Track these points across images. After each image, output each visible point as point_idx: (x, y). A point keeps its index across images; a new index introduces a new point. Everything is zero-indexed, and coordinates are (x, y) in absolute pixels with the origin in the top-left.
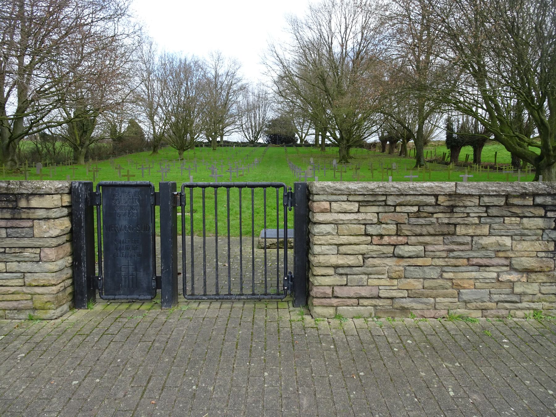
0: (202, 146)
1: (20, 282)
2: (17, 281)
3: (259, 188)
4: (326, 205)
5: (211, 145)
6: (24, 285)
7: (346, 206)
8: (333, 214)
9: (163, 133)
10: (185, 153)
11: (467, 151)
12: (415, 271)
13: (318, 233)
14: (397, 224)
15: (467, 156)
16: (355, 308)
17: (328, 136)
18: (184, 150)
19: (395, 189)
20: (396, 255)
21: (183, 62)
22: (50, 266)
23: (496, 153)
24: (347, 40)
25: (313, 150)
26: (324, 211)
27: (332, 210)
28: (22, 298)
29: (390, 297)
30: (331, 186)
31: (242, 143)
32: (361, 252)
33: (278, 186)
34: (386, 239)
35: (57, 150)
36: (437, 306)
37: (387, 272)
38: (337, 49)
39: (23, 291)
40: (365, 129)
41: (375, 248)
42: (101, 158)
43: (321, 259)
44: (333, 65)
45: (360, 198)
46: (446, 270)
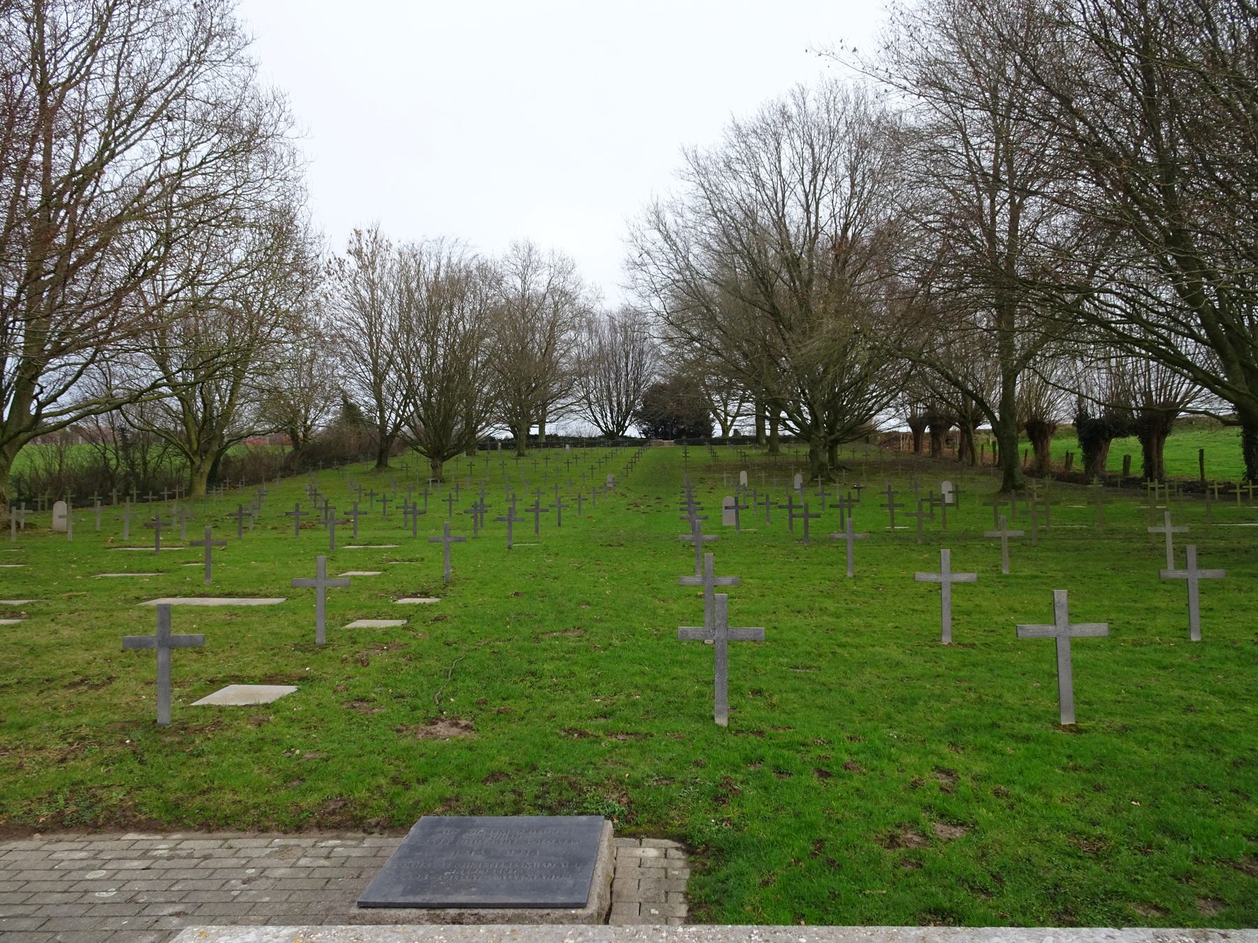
0: (494, 447)
10: (449, 466)
15: (1127, 460)
17: (784, 419)
18: (444, 459)
23: (1202, 452)
24: (819, 199)
25: (748, 452)
31: (590, 438)
35: (152, 465)
38: (794, 213)
40: (870, 400)
44: (793, 263)
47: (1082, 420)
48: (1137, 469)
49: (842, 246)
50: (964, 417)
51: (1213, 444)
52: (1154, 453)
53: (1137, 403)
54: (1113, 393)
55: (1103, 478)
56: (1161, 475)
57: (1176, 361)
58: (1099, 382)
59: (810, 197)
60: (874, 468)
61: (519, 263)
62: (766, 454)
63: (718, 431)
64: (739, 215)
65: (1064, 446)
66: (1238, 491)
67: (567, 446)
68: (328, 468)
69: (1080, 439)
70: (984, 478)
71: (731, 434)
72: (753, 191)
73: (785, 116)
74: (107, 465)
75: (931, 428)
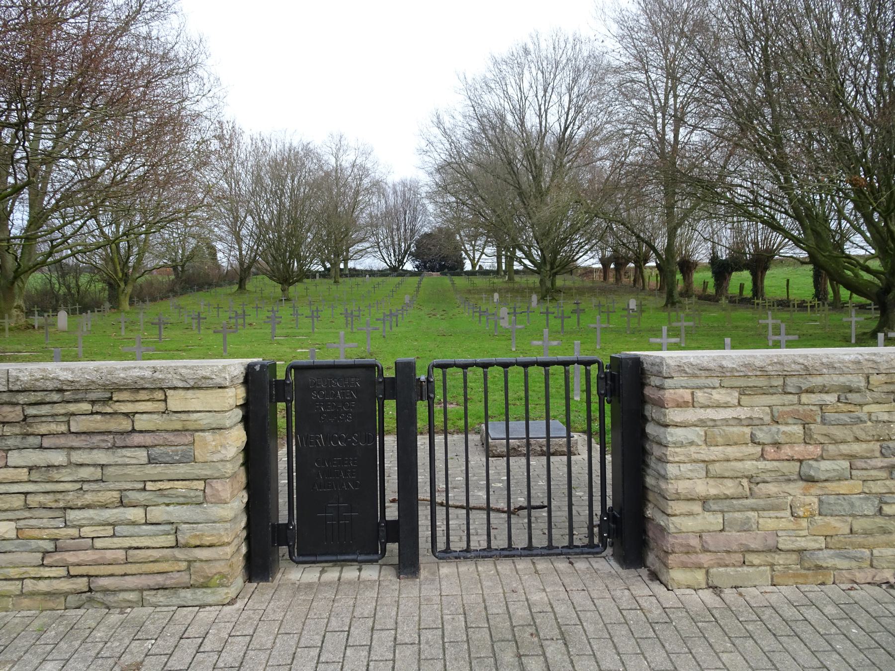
0: (314, 277)
1: (170, 540)
2: (163, 538)
3: (556, 366)
4: (686, 395)
5: (329, 275)
6: (177, 546)
7: (718, 396)
8: (698, 410)
9: (255, 256)
10: (291, 289)
11: (741, 279)
12: (837, 504)
13: (675, 443)
14: (804, 425)
15: (742, 287)
16: (739, 569)
18: (290, 284)
19: (798, 367)
20: (803, 477)
21: (287, 145)
22: (221, 510)
23: (788, 281)
26: (682, 405)
27: (695, 404)
28: (171, 569)
29: (796, 549)
30: (694, 363)
32: (746, 474)
33: (587, 363)
34: (787, 451)
35: (82, 288)
36: (875, 563)
37: (789, 507)
38: (532, 121)
39: (175, 557)
41: (770, 465)
42: (153, 299)
43: (682, 486)
44: (530, 155)
45: (742, 383)
46: (888, 501)
47: (714, 261)
48: (748, 292)
49: (563, 142)
50: (638, 257)
51: (795, 276)
52: (759, 281)
53: (749, 249)
54: (734, 242)
55: (727, 297)
56: (762, 296)
57: (776, 227)
58: (726, 235)
60: (581, 291)
61: (334, 146)
62: (506, 282)
63: (468, 266)
64: (495, 120)
65: (703, 277)
66: (809, 305)
67: (367, 276)
68: (185, 294)
69: (713, 273)
70: (651, 298)
71: (477, 268)
72: (502, 101)
73: (526, 52)
74: (52, 288)
75: (615, 265)
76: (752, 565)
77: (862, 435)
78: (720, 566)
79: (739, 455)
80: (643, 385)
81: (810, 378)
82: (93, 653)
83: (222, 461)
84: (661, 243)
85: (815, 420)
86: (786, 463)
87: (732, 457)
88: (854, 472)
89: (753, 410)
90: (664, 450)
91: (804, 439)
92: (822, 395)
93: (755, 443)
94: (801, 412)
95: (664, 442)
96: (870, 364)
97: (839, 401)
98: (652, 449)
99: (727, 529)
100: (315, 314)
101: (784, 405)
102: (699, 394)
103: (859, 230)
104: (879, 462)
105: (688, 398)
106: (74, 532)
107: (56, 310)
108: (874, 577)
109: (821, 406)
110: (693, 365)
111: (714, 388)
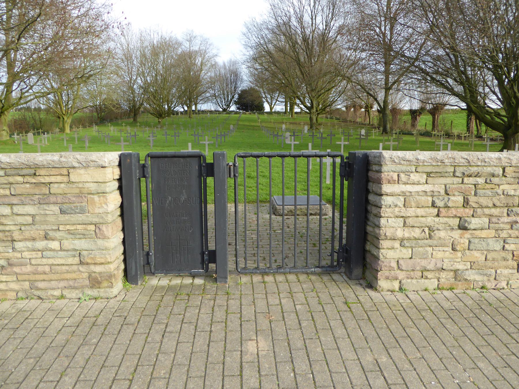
7: (415, 177)
16: (420, 281)
33: (334, 157)
34: (453, 212)
38: (307, 18)
44: (305, 39)
45: (429, 170)
48: (429, 128)
59: (313, 13)
66: (463, 135)
76: (427, 278)
77: (498, 204)
78: (408, 278)
79: (424, 214)
80: (368, 170)
81: (470, 168)
82: (32, 325)
83: (105, 213)
84: (381, 96)
85: (471, 193)
86: (451, 219)
87: (420, 215)
88: (491, 225)
89: (434, 187)
90: (378, 209)
91: (463, 205)
92: (476, 178)
93: (434, 207)
94: (463, 188)
95: (379, 205)
96: (506, 160)
97: (486, 182)
98: (371, 209)
99: (414, 257)
100: (177, 134)
101: (453, 184)
102: (402, 175)
103: (494, 93)
104: (506, 219)
105: (395, 177)
106: (19, 255)
107: (27, 132)
108: (496, 285)
109: (475, 185)
110: (399, 157)
111: (412, 172)
